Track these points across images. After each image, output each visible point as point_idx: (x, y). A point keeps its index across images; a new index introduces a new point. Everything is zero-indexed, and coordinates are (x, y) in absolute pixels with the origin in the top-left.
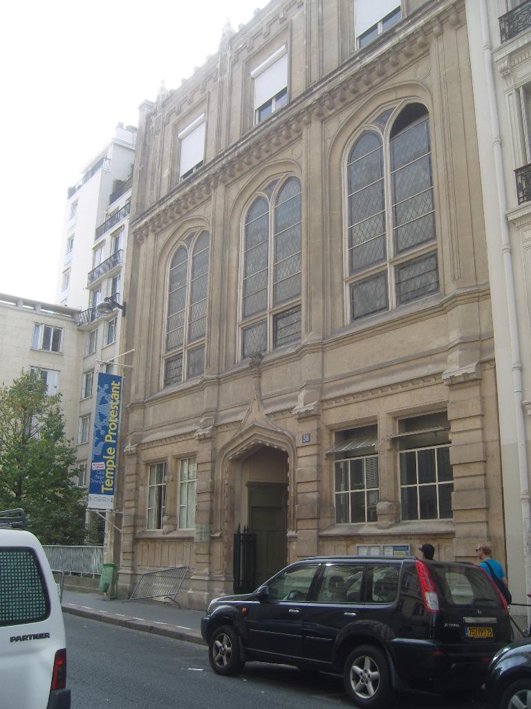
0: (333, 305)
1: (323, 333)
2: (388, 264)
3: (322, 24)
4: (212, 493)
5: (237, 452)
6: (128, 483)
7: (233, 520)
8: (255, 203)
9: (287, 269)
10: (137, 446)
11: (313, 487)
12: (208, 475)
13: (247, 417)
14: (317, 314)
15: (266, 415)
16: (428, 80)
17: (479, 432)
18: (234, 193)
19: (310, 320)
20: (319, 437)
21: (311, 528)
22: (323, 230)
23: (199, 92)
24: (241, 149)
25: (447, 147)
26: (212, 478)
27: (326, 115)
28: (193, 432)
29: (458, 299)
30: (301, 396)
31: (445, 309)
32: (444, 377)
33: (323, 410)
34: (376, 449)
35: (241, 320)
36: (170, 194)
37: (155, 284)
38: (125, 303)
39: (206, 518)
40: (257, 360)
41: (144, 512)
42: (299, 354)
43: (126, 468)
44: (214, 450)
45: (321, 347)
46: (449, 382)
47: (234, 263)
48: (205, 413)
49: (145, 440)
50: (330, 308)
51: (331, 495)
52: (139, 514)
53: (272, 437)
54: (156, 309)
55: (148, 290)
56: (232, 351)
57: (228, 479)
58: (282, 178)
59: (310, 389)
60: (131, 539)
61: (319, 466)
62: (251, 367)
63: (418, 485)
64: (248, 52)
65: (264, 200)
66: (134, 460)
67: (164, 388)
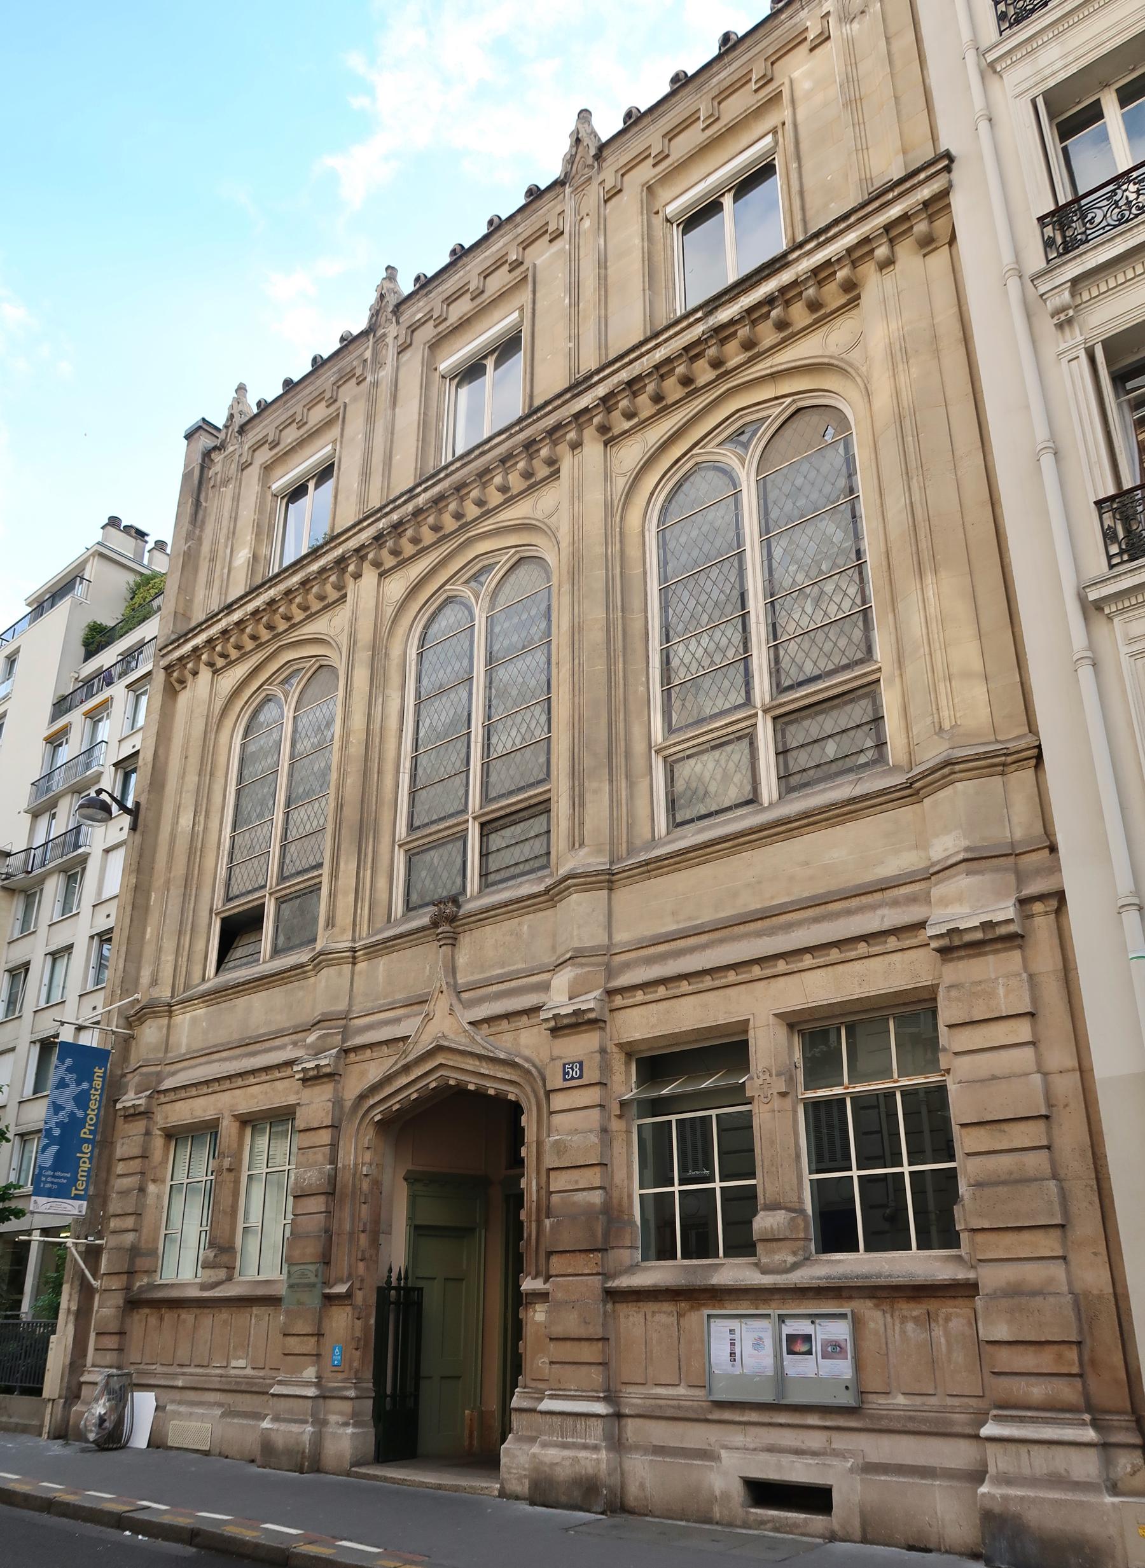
0: (631, 797)
1: (611, 853)
2: (470, 820)
3: (606, 268)
4: (330, 1194)
5: (395, 1104)
6: (119, 1176)
7: (377, 1255)
8: (440, 609)
9: (513, 734)
10: (150, 1097)
11: (593, 1177)
12: (321, 1156)
13: (420, 1031)
14: (597, 812)
15: (470, 1023)
16: (855, 356)
17: (1029, 1052)
18: (396, 587)
19: (582, 824)
20: (605, 1067)
21: (586, 1271)
22: (608, 649)
23: (323, 404)
24: (421, 500)
25: (913, 473)
26: (333, 1161)
27: (616, 431)
28: (289, 1063)
29: (957, 767)
30: (561, 981)
31: (917, 792)
32: (931, 931)
33: (611, 1011)
34: (749, 1094)
35: (404, 835)
36: (253, 591)
37: (207, 768)
38: (137, 804)
39: (311, 1249)
40: (450, 909)
41: (155, 1240)
42: (552, 896)
43: (119, 1145)
44: (337, 1102)
45: (608, 880)
46: (552, 1024)
47: (393, 723)
48: (319, 1022)
49: (167, 1084)
50: (624, 802)
51: (630, 1196)
52: (143, 1245)
53: (483, 1071)
54: (207, 816)
55: (192, 779)
56: (383, 896)
57: (371, 1164)
58: (505, 560)
59: (582, 965)
60: (121, 1302)
61: (604, 1130)
62: (435, 924)
63: (717, 1185)
64: (435, 327)
65: (462, 603)
66: (139, 1126)
67: (271, 957)
